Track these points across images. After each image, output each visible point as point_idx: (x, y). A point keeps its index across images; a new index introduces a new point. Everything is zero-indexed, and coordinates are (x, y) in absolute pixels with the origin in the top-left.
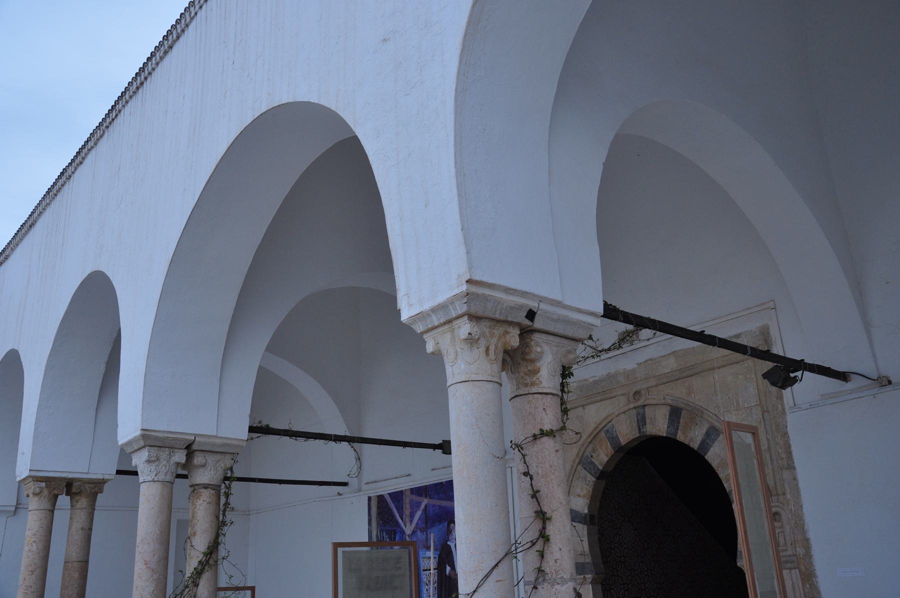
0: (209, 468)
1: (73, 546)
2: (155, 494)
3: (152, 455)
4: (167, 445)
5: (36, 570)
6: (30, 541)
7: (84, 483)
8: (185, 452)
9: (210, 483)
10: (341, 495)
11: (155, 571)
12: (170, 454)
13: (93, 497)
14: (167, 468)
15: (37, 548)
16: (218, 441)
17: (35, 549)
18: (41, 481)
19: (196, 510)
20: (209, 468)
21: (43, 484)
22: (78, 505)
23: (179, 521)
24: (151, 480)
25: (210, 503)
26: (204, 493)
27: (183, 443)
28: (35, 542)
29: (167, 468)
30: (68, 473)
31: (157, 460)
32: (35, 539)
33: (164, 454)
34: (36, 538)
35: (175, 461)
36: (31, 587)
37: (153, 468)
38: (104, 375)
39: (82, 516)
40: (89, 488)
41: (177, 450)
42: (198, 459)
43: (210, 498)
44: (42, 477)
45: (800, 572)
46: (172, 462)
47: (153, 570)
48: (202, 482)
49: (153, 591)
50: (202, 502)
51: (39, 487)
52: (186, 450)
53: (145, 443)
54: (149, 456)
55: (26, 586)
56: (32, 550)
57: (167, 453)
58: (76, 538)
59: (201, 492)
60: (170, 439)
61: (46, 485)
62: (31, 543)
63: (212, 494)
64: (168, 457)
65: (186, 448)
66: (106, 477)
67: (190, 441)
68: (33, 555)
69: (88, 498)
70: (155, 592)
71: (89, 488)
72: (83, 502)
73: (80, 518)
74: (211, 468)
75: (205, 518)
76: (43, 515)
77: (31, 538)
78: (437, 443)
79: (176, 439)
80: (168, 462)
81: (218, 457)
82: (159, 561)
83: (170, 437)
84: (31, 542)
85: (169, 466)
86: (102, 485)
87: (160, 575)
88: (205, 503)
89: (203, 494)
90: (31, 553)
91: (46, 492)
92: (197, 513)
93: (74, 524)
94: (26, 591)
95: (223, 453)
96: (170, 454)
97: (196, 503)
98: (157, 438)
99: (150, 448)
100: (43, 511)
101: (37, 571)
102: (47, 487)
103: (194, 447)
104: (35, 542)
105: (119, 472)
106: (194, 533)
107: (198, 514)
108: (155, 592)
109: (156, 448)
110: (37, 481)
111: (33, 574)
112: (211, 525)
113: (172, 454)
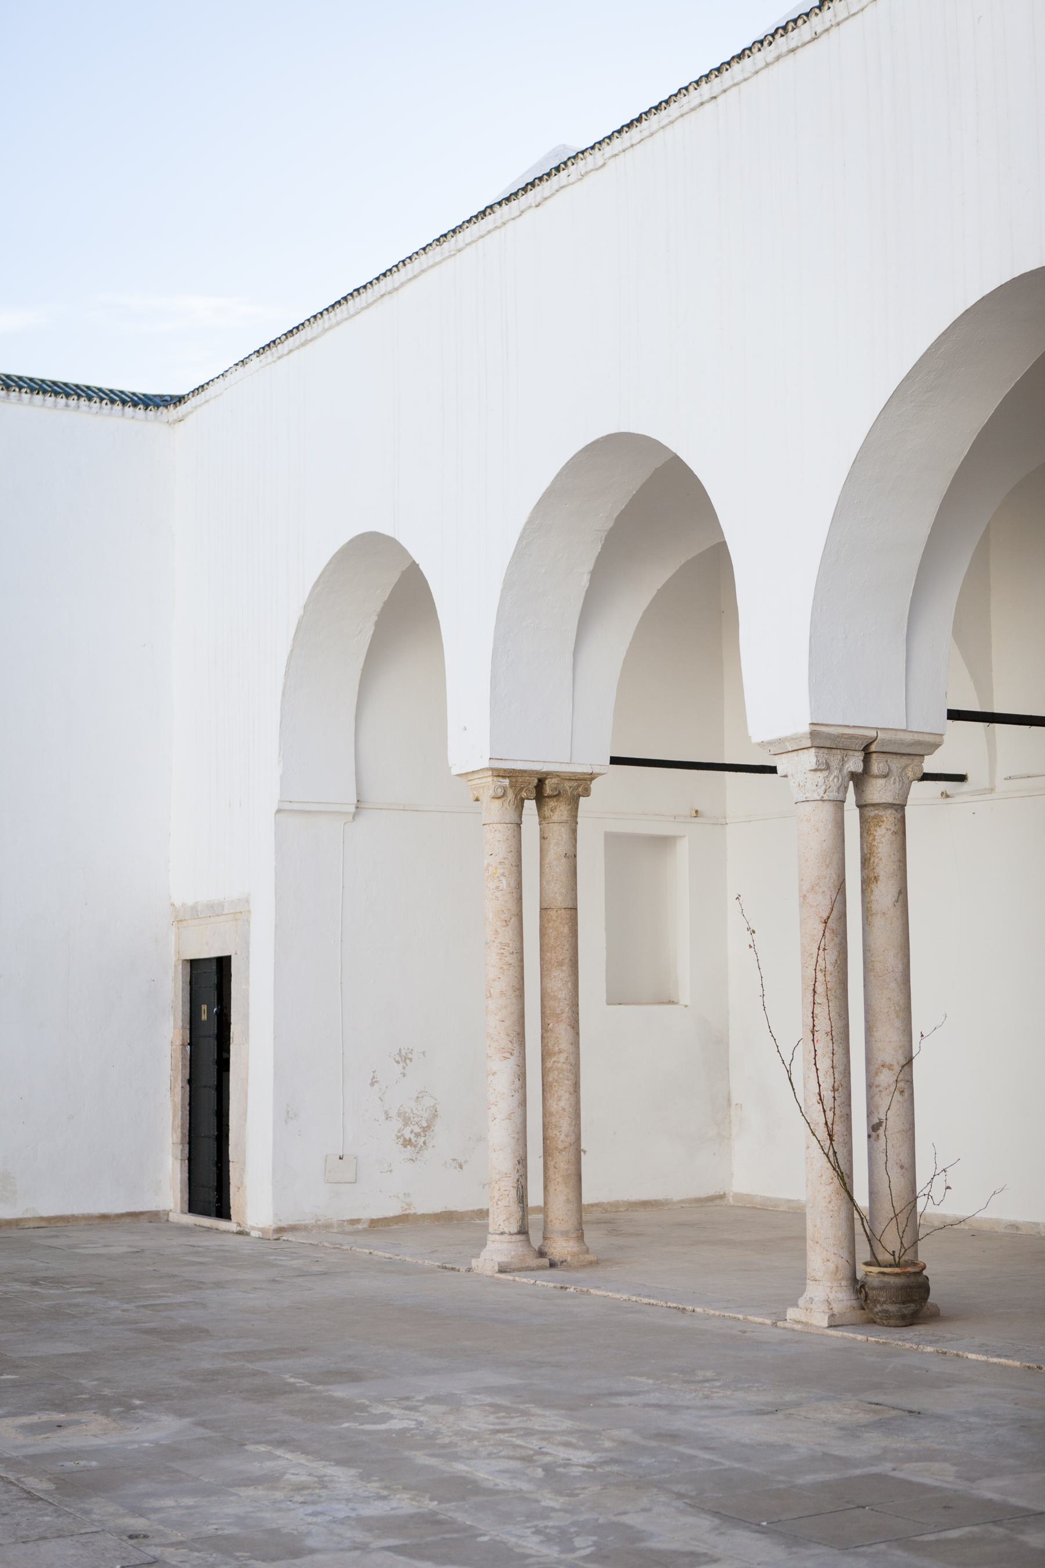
0: (892, 779)
1: (556, 883)
2: (826, 820)
3: (821, 761)
4: (840, 745)
5: (511, 919)
6: (495, 873)
7: (563, 779)
8: (860, 756)
9: (894, 802)
10: (947, 796)
11: (835, 932)
12: (843, 759)
13: (574, 802)
14: (840, 780)
15: (509, 884)
16: (908, 737)
17: (505, 887)
18: (503, 777)
19: (875, 843)
20: (892, 779)
21: (506, 782)
22: (556, 817)
23: (612, 839)
24: (819, 798)
25: (896, 833)
26: (887, 818)
27: (860, 742)
28: (503, 875)
29: (840, 780)
30: (542, 764)
31: (827, 769)
32: (502, 871)
33: (835, 759)
34: (504, 868)
35: (849, 769)
36: (508, 945)
37: (821, 781)
38: (587, 591)
39: (564, 836)
40: (570, 787)
41: (851, 753)
42: (877, 765)
43: (895, 825)
44: (505, 770)
45: (412, 1429)
46: (845, 771)
47: (833, 930)
48: (883, 801)
49: (836, 960)
50: (884, 831)
51: (500, 786)
52: (863, 753)
53: (812, 743)
54: (818, 764)
55: (501, 943)
56: (501, 889)
57: (839, 757)
58: (558, 870)
59: (882, 816)
60: (845, 736)
61: (510, 781)
62: (498, 877)
63: (898, 820)
64: (841, 764)
65: (863, 750)
66: (596, 770)
67: (871, 738)
68: (504, 895)
69: (569, 805)
70: (839, 962)
71: (570, 787)
72: (559, 811)
73: (560, 838)
74: (895, 779)
75: (890, 856)
76: (510, 832)
77: (496, 868)
78: (612, 525)
79: (852, 737)
80: (841, 770)
81: (904, 760)
82: (840, 918)
83: (846, 734)
84: (497, 875)
85: (842, 777)
86: (589, 783)
87: (842, 937)
88: (890, 832)
89: (885, 819)
90: (500, 893)
91: (510, 795)
92: (877, 848)
93: (551, 847)
94: (502, 951)
95: (910, 755)
96: (843, 760)
97: (875, 833)
98: (829, 736)
99: (817, 750)
100: (509, 825)
101: (513, 919)
102: (511, 787)
103: (873, 748)
104: (503, 875)
105: (615, 761)
106: (875, 878)
107: (880, 850)
108: (839, 962)
109: (826, 751)
110: (498, 776)
111: (507, 925)
112: (900, 866)
113: (846, 759)
